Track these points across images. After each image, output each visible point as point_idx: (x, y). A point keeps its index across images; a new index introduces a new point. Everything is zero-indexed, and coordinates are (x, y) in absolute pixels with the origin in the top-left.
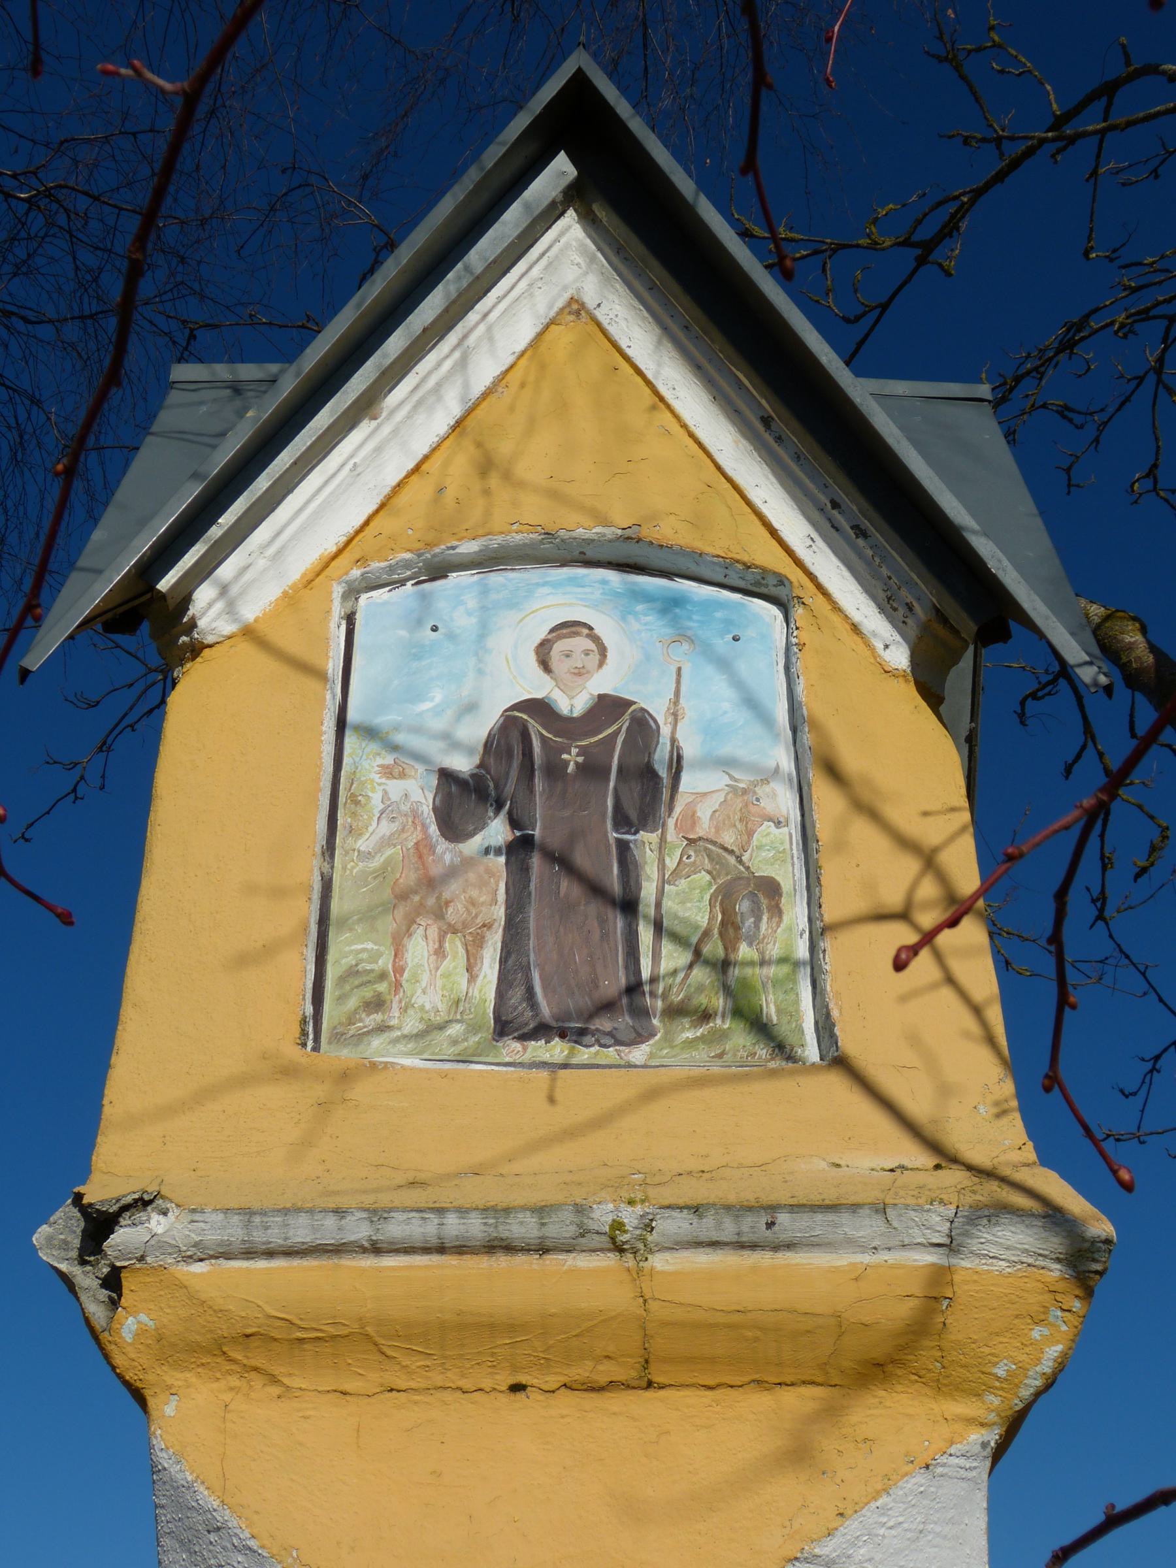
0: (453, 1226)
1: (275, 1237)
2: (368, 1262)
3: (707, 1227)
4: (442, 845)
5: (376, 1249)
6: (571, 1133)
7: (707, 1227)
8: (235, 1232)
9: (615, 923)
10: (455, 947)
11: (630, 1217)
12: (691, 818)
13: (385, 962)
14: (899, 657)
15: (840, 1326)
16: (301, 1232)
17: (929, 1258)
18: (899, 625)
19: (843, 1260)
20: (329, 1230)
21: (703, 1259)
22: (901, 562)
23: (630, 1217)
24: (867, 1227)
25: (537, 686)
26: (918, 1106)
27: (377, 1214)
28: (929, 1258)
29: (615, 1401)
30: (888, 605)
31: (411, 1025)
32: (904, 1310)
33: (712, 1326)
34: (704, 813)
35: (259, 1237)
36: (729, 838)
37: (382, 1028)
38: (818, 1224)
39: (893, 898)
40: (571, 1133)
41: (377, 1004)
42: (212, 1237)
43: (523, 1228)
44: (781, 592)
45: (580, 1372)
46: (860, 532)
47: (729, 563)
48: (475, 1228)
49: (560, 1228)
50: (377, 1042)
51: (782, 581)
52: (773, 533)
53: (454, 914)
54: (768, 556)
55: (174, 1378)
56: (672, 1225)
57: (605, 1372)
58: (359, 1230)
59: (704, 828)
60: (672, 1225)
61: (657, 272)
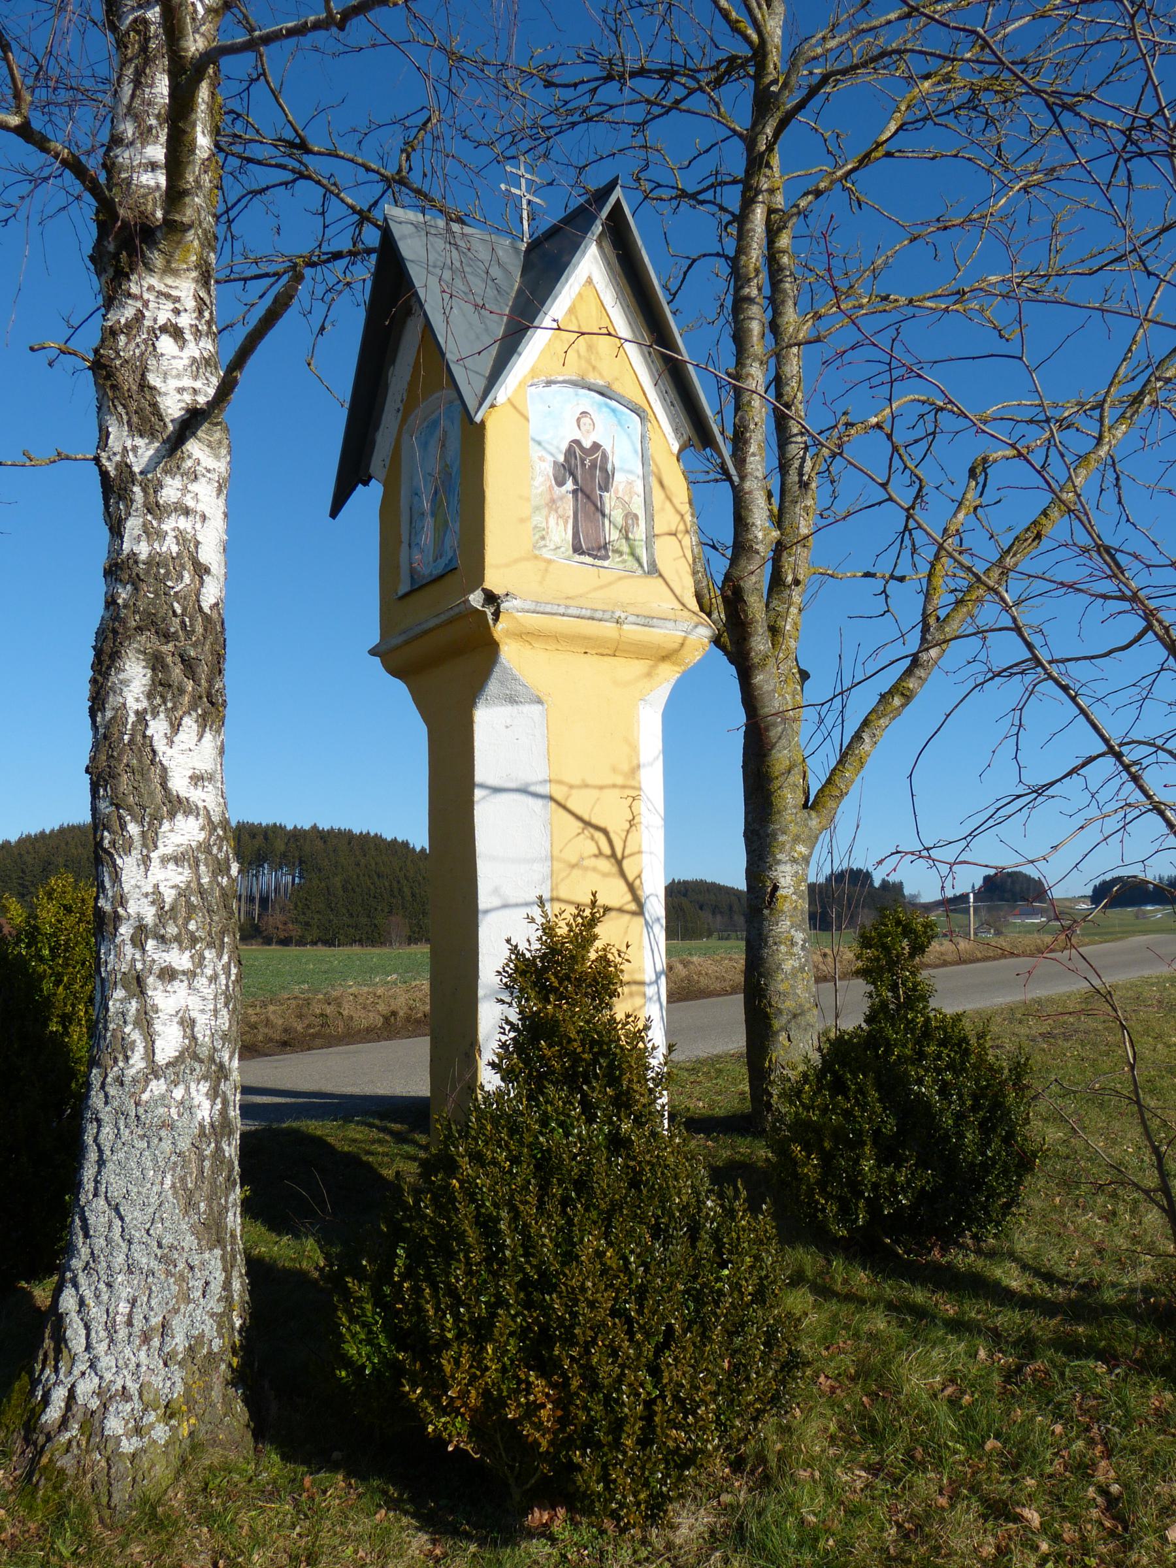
0: (584, 612)
1: (541, 609)
2: (560, 618)
3: (639, 620)
4: (556, 488)
5: (563, 615)
6: (601, 587)
7: (639, 620)
8: (532, 607)
9: (603, 524)
10: (561, 522)
11: (623, 616)
12: (617, 492)
13: (544, 525)
14: (676, 447)
15: (659, 647)
16: (548, 609)
17: (683, 634)
18: (678, 439)
19: (662, 631)
20: (555, 609)
21: (634, 627)
22: (683, 418)
23: (623, 616)
24: (670, 625)
25: (577, 435)
26: (678, 592)
27: (567, 607)
28: (683, 634)
29: (606, 658)
30: (676, 430)
31: (553, 547)
32: (676, 646)
33: (589, 638)
34: (620, 489)
35: (538, 609)
36: (626, 499)
37: (545, 546)
38: (661, 623)
39: (673, 529)
40: (601, 587)
41: (543, 538)
42: (527, 607)
43: (599, 615)
44: (642, 414)
45: (600, 651)
46: (673, 405)
47: (630, 402)
48: (588, 613)
49: (607, 616)
50: (544, 550)
51: (644, 411)
52: (645, 394)
53: (560, 511)
54: (640, 401)
55: (508, 641)
56: (632, 619)
57: (606, 651)
58: (562, 610)
59: (620, 495)
60: (632, 619)
61: (623, 281)
